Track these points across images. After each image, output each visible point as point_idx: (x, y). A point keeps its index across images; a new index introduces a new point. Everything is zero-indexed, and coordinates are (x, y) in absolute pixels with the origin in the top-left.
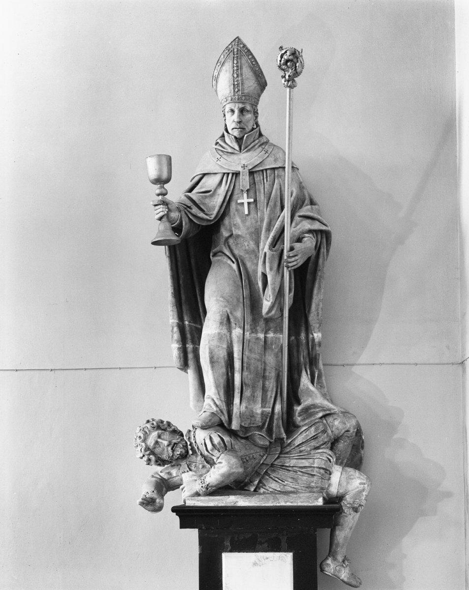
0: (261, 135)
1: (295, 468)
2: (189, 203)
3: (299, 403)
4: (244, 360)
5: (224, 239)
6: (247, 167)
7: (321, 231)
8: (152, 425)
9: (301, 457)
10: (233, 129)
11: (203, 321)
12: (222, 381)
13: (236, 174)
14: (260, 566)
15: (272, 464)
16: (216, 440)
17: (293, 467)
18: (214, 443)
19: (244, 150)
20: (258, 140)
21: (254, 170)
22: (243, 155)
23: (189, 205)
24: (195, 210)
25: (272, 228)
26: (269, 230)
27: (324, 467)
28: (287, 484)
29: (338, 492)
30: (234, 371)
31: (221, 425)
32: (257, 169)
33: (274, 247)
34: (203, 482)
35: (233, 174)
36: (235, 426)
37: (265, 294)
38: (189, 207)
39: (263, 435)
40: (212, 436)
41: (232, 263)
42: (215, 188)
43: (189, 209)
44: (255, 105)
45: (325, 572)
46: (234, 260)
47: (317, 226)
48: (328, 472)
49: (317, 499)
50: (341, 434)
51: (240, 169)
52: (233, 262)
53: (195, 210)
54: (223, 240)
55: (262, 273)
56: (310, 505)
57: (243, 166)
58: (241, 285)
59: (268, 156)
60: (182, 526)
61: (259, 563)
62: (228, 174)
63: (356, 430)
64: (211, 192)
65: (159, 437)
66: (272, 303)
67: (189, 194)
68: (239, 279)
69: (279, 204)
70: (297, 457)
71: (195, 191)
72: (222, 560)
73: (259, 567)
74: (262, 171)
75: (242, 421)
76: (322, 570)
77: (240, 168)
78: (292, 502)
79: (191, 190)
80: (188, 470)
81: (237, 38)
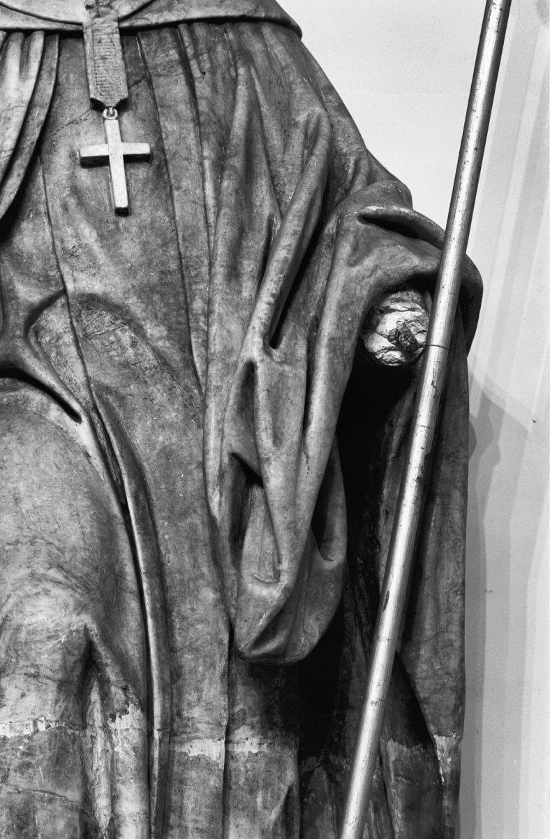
5: (23, 314)
35: (48, 34)
52: (75, 417)
55: (234, 456)
62: (28, 33)
74: (173, 26)
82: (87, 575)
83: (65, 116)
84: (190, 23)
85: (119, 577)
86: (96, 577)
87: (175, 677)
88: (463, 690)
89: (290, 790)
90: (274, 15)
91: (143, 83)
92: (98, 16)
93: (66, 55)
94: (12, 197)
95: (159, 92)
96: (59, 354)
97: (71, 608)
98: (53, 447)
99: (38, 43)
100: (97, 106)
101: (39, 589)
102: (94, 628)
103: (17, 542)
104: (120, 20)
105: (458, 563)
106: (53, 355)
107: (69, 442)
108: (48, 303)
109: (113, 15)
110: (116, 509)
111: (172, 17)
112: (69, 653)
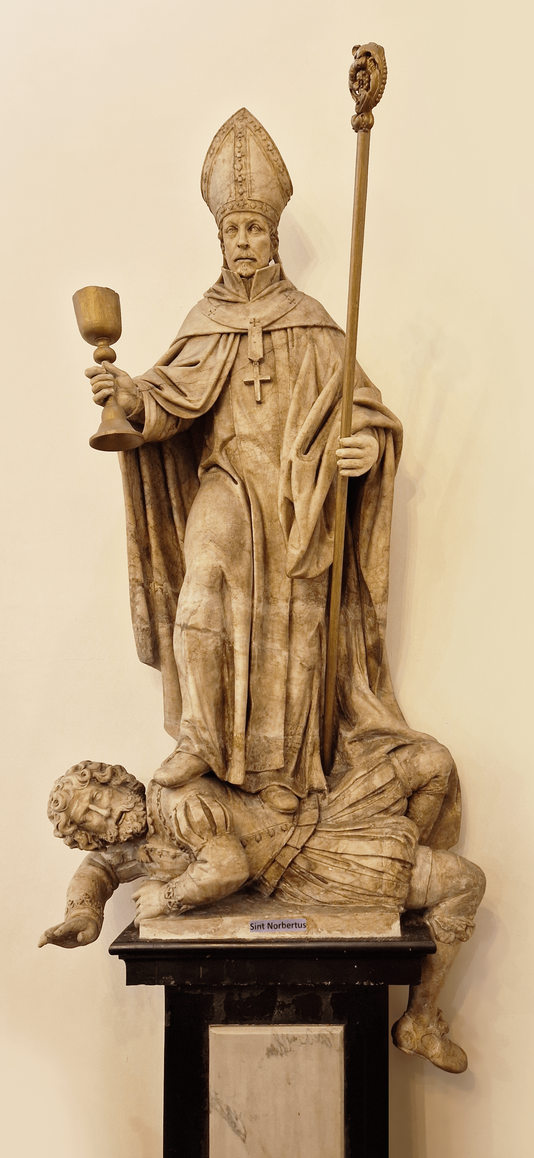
0: (282, 277)
1: (346, 857)
2: (159, 381)
3: (351, 724)
4: (253, 654)
5: (220, 443)
6: (259, 322)
7: (387, 430)
8: (80, 779)
9: (357, 833)
10: (236, 260)
11: (174, 605)
12: (213, 692)
13: (243, 335)
14: (281, 1055)
15: (304, 848)
16: (197, 814)
17: (342, 854)
18: (191, 820)
19: (253, 298)
20: (278, 283)
21: (271, 328)
22: (253, 304)
23: (158, 383)
24: (169, 392)
25: (301, 422)
26: (295, 425)
27: (400, 857)
28: (332, 887)
29: (426, 902)
30: (233, 675)
31: (209, 774)
32: (276, 326)
33: (306, 453)
34: (171, 895)
35: (236, 334)
36: (236, 776)
37: (290, 537)
38: (158, 387)
39: (288, 786)
40: (191, 805)
41: (232, 483)
42: (204, 358)
43: (158, 390)
44: (274, 222)
45: (403, 1049)
46: (236, 478)
47: (378, 419)
48: (408, 866)
49: (389, 925)
50: (424, 784)
51: (246, 325)
52: (236, 483)
53: (169, 392)
54: (217, 445)
55: (286, 498)
56: (375, 935)
57: (253, 325)
58: (249, 522)
59: (295, 308)
60: (132, 979)
61: (279, 1049)
62: (228, 334)
63: (449, 774)
64: (199, 365)
65: (92, 800)
66: (302, 552)
67: (163, 368)
68: (245, 510)
69: (312, 383)
70: (349, 834)
71: (175, 363)
72: (208, 1040)
73: (279, 1056)
74: (285, 329)
75: (248, 767)
76: (397, 1043)
77: (249, 324)
78: (341, 931)
79: (168, 362)
80: (148, 860)
81: (242, 109)
82: (225, 545)
83: (239, 366)
84: (292, 328)
85: (242, 545)
86: (229, 545)
87: (266, 583)
88: (387, 587)
89: (319, 624)
90: (329, 324)
91: (272, 352)
92: (255, 326)
93: (243, 342)
94: (217, 397)
95: (277, 356)
96: (234, 458)
97: (214, 558)
98: (225, 494)
99: (231, 337)
100: (252, 361)
101: (204, 550)
102: (224, 566)
103: (201, 531)
104: (263, 328)
105: (387, 538)
106: (232, 458)
107: (231, 492)
108: (231, 438)
109: (261, 326)
110: (247, 518)
111: (285, 326)
112: (212, 576)
